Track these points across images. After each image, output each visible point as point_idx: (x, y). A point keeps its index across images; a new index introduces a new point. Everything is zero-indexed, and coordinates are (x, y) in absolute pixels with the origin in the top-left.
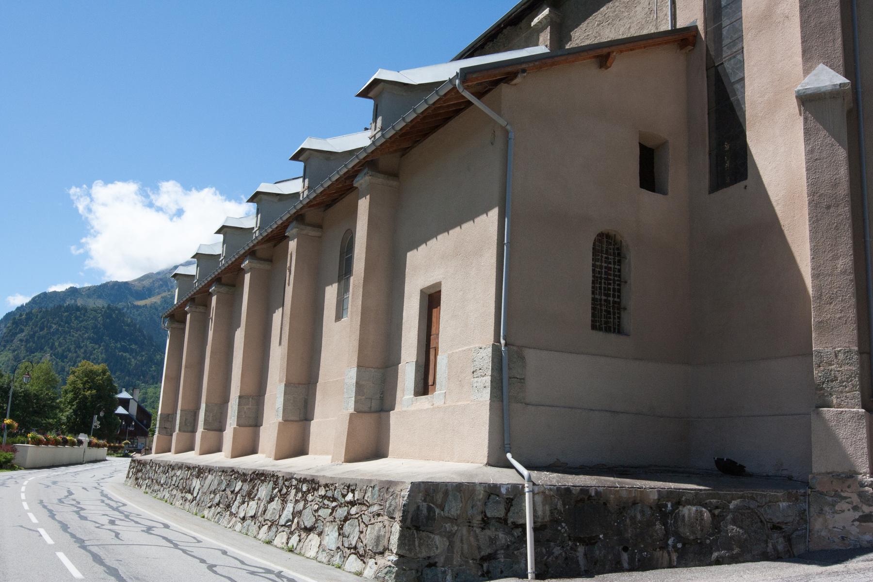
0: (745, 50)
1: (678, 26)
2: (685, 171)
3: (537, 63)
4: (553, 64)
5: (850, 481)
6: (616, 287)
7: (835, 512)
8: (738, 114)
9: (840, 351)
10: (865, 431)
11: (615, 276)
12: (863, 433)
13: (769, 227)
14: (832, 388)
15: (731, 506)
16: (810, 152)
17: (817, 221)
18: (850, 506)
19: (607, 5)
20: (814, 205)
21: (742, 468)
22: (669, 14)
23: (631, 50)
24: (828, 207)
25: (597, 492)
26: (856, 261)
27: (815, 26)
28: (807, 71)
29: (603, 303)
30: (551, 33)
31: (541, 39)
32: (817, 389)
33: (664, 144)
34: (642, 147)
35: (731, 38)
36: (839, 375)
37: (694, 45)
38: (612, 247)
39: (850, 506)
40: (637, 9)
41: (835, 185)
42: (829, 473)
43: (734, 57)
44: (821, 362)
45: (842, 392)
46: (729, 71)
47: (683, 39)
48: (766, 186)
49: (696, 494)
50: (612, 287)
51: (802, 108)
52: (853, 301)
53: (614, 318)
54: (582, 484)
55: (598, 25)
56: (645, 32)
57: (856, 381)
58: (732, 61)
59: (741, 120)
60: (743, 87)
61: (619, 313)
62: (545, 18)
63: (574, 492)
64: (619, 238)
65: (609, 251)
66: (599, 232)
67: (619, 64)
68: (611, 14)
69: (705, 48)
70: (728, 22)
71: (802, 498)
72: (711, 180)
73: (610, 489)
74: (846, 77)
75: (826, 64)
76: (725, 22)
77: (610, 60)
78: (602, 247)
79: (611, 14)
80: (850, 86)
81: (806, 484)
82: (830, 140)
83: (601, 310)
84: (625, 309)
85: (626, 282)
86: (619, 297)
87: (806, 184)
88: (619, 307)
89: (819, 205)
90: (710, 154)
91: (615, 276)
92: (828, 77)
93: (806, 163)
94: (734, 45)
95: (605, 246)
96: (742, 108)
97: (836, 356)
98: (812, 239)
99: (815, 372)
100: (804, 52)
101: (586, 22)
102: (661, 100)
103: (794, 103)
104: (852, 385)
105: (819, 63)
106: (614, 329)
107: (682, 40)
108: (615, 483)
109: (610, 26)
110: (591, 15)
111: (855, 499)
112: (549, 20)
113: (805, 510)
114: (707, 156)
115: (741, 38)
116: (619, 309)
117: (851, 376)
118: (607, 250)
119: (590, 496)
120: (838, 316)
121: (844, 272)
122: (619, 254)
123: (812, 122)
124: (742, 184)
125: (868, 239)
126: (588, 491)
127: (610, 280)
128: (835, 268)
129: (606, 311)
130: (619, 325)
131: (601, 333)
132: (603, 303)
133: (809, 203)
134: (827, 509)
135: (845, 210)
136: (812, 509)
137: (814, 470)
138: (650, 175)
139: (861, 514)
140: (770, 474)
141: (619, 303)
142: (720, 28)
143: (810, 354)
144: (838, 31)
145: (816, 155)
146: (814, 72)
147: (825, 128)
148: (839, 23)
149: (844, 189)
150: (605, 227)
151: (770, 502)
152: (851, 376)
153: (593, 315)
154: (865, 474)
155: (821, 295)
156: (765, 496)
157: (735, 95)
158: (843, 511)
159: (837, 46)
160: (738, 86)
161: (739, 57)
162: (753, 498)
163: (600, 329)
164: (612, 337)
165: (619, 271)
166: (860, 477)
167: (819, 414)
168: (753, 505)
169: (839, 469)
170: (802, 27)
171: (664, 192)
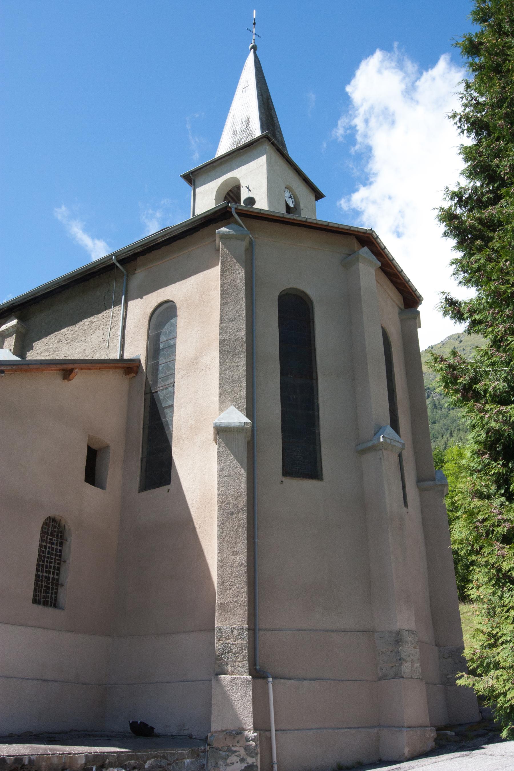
0: (175, 384)
1: (125, 357)
2: (122, 470)
3: (14, 367)
4: (26, 370)
5: (239, 737)
6: (57, 566)
7: (227, 765)
8: (167, 432)
9: (235, 628)
10: (251, 694)
11: (56, 555)
12: (249, 696)
13: (185, 525)
14: (228, 658)
15: (146, 766)
16: (221, 470)
17: (224, 523)
18: (238, 759)
19: (68, 328)
20: (222, 511)
21: (152, 728)
22: (119, 345)
23: (89, 369)
24: (232, 514)
25: (30, 761)
26: (248, 557)
27: (229, 377)
28: (222, 409)
29: (44, 579)
30: (15, 340)
31: (6, 343)
32: (217, 659)
33: (106, 448)
34: (89, 449)
35: (165, 373)
36: (233, 647)
37: (136, 373)
38: (56, 530)
39: (238, 759)
40: (93, 336)
41: (238, 497)
42: (223, 731)
43: (167, 388)
44: (221, 637)
45: (235, 662)
46: (161, 398)
47: (129, 367)
48: (185, 492)
49: (118, 756)
50: (52, 565)
51: (217, 436)
52: (246, 588)
53: (52, 593)
54: (16, 753)
55: (58, 342)
56: (97, 357)
57: (245, 652)
58: (165, 391)
59: (169, 438)
60: (172, 412)
61: (57, 589)
62: (12, 327)
63: (8, 761)
64: (63, 523)
65: (54, 532)
66: (48, 516)
67: (79, 379)
68: (70, 336)
69: (145, 378)
70: (164, 361)
71: (202, 754)
72: (141, 481)
73: (42, 757)
74: (247, 416)
75: (235, 406)
76: (162, 361)
77: (73, 374)
78: (48, 530)
79: (70, 336)
80: (251, 425)
81: (205, 740)
82: (235, 463)
83: (42, 585)
84: (62, 585)
85: (65, 562)
86: (58, 574)
87: (216, 495)
88: (57, 583)
89: (225, 512)
90: (142, 461)
91: (56, 555)
92: (236, 417)
93: (218, 478)
94: (167, 379)
95: (50, 529)
96: (169, 429)
97: (232, 632)
98: (220, 537)
99: (216, 645)
100: (221, 395)
101: (48, 338)
102: (107, 413)
103: (210, 432)
104: (243, 655)
105: (231, 405)
106: (51, 603)
107: (128, 368)
108: (46, 750)
109: (68, 345)
110: (52, 333)
111: (242, 752)
112: (15, 329)
113: (204, 765)
114: (140, 462)
115: (173, 375)
116: (57, 585)
117: (242, 649)
118: (51, 533)
119: (24, 765)
120: (235, 599)
121: (240, 565)
122: (61, 536)
123: (224, 448)
124: (166, 487)
125: (256, 540)
126: (21, 760)
127: (52, 558)
128: (234, 561)
129: (45, 586)
130: (55, 600)
131: (40, 607)
132: (44, 579)
133: (219, 509)
134: (221, 762)
135: (243, 517)
136: (209, 764)
137: (213, 729)
138: (92, 475)
139: (246, 765)
140: (174, 734)
141: (58, 580)
142: (157, 365)
143: (213, 629)
144: (244, 384)
145: (225, 473)
146: (227, 411)
147: (232, 453)
148: (245, 378)
149: (243, 501)
150: (52, 513)
151: (177, 759)
152: (242, 649)
153: (35, 590)
154: (250, 730)
155: (223, 582)
156: (174, 754)
157: (165, 417)
158: (233, 764)
159: (243, 394)
160: (167, 411)
161: (170, 389)
162: (164, 757)
163: (39, 603)
164: (50, 610)
165: (61, 551)
166: (246, 733)
167: (218, 680)
168: (164, 763)
169: (231, 727)
170: (220, 377)
171: (102, 486)
